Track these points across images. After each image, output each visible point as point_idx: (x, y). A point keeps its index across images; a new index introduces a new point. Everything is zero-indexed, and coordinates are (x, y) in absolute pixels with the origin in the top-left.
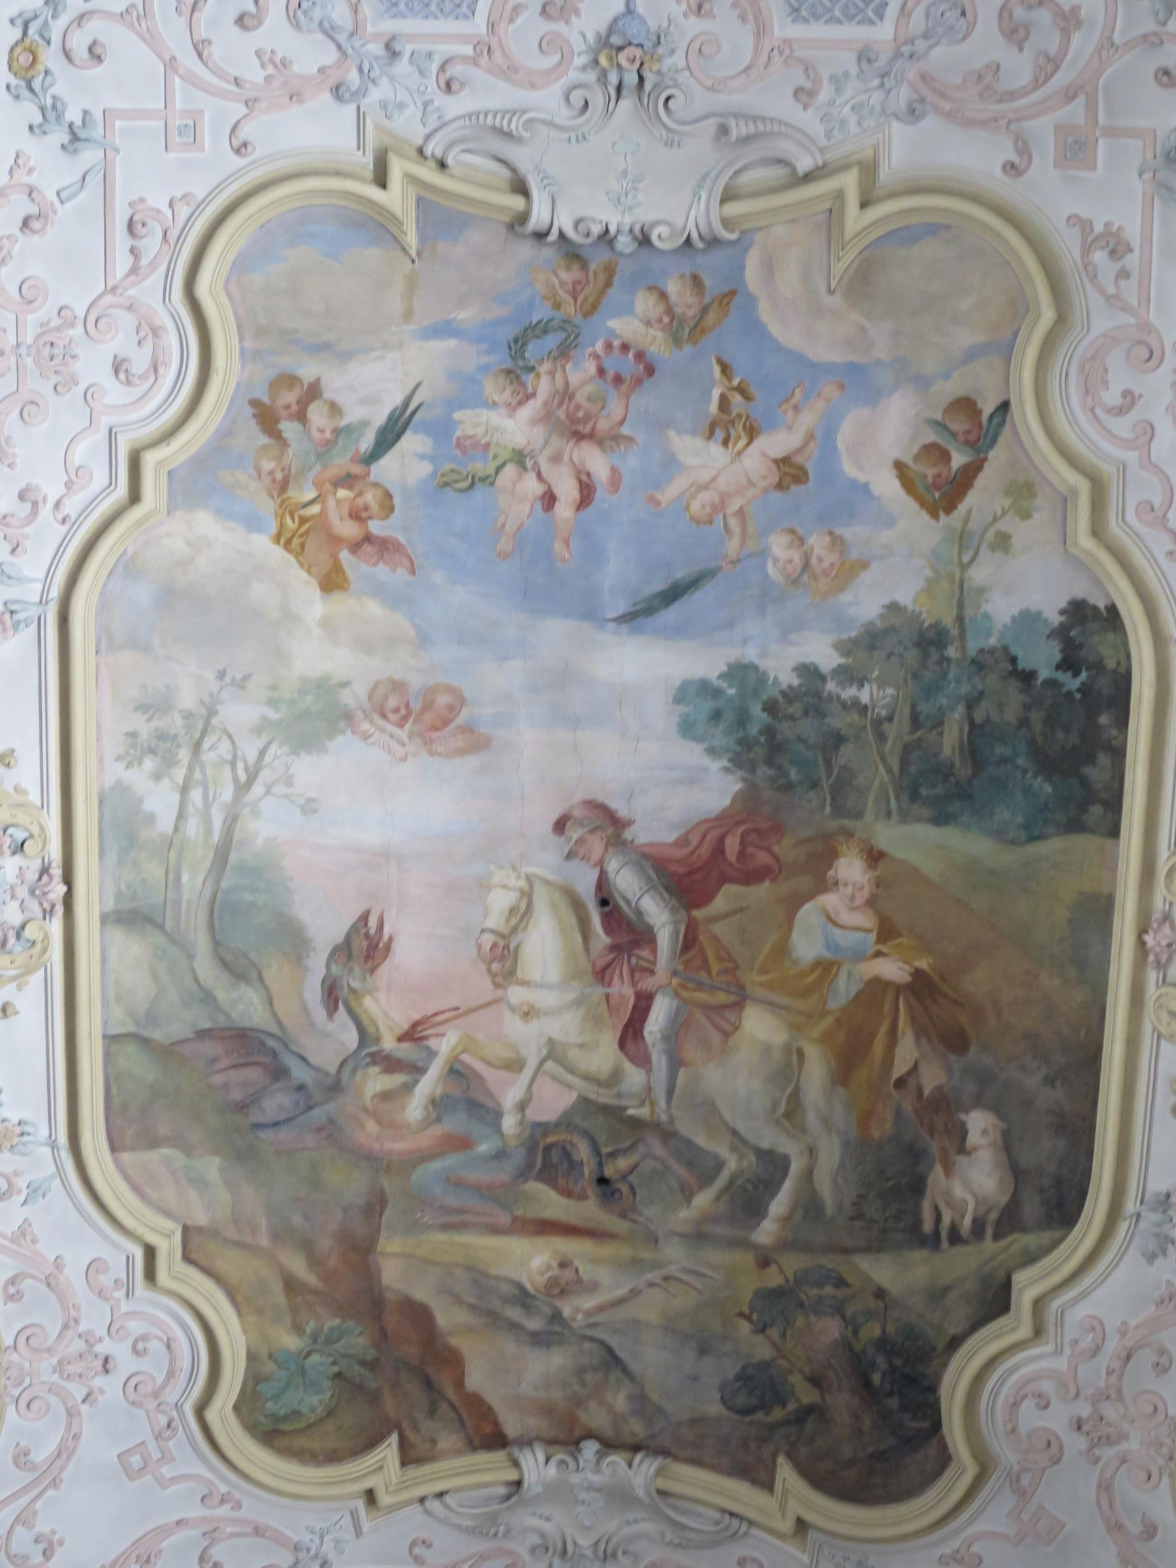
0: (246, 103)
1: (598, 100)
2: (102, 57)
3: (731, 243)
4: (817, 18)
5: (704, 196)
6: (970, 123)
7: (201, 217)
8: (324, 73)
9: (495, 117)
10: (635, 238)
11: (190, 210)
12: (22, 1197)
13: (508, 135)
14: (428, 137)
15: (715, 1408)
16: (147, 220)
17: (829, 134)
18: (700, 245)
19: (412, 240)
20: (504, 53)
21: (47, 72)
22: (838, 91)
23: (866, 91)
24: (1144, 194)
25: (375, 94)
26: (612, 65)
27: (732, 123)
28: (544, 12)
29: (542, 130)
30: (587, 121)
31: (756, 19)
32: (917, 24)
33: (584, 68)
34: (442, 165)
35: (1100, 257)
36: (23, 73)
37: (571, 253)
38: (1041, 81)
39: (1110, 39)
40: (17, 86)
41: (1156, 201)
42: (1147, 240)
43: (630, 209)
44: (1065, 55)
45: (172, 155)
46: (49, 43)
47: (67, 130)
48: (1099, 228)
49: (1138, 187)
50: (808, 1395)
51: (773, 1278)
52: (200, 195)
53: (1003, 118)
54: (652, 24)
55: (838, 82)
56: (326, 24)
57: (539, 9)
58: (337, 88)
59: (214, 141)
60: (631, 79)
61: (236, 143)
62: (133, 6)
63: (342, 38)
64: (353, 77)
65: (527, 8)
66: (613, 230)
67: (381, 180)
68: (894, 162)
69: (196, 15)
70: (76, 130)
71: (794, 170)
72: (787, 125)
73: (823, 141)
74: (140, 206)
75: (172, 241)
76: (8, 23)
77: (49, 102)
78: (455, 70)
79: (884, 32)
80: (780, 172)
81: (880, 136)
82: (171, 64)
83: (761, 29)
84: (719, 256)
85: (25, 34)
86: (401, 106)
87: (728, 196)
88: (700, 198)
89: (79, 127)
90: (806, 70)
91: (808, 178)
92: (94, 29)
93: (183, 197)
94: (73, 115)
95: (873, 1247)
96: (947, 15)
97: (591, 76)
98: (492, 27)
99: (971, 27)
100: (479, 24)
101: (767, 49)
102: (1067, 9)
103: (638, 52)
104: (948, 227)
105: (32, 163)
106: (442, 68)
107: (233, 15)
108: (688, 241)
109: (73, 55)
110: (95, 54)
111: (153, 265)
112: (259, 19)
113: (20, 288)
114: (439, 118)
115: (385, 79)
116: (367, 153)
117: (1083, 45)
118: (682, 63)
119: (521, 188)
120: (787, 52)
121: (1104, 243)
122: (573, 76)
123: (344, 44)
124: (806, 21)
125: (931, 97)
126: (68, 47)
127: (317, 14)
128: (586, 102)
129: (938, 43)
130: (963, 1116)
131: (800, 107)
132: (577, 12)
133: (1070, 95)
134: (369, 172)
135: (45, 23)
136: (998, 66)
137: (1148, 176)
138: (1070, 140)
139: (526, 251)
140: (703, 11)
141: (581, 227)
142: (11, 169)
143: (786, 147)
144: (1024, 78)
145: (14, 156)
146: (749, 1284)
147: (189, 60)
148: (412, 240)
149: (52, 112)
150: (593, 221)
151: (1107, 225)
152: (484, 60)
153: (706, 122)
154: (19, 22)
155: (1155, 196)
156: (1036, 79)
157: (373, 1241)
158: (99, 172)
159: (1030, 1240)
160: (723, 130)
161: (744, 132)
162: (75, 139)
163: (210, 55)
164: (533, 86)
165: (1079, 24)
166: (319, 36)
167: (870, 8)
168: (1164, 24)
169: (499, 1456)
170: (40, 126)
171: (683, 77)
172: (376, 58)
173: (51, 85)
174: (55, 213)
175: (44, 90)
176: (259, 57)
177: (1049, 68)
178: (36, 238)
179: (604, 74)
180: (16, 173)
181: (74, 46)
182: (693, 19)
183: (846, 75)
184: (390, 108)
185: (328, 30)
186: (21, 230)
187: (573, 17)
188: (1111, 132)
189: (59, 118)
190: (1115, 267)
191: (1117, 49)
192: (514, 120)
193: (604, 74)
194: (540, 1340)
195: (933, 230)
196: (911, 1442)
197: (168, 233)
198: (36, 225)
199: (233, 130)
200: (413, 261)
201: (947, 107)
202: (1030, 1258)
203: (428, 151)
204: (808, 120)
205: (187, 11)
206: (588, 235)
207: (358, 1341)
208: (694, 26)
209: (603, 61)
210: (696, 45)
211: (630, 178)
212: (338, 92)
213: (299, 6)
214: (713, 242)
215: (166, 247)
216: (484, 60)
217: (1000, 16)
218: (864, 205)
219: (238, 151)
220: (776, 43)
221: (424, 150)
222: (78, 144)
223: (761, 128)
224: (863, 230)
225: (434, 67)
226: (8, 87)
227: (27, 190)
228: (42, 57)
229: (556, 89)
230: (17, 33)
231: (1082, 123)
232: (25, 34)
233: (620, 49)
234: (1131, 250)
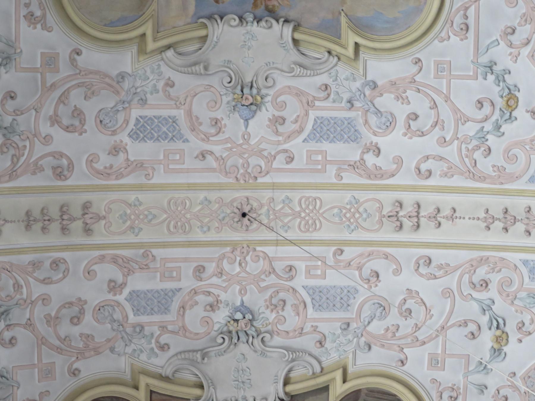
0: (415, 81)
1: (261, 82)
2: (477, 102)
3: (202, 18)
4: (165, 119)
5: (215, 39)
6: (97, 73)
7: (436, 32)
8: (381, 94)
9: (306, 74)
10: (245, 19)
11: (441, 35)
13: (301, 66)
14: (336, 65)
16: (460, 31)
17: (159, 66)
18: (216, 16)
19: (343, 20)
20: (301, 101)
21: (502, 97)
22: (155, 86)
23: (143, 86)
24: (19, 43)
25: (358, 84)
26: (255, 96)
27: (202, 71)
28: (284, 120)
29: (285, 68)
30: (265, 71)
31: (192, 118)
32: (121, 117)
33: (267, 95)
34: (329, 52)
35: (38, 13)
36: (513, 96)
37: (272, 13)
38: (66, 93)
39: (37, 112)
40: (515, 91)
41: (13, 38)
42: (17, 21)
43: (247, 33)
44: (56, 104)
45: (448, 59)
46: (501, 109)
47: (494, 71)
48: (39, 26)
49: (22, 45)
52: (436, 41)
53: (83, 75)
54: (237, 115)
55: (155, 90)
56: (379, 115)
57: (286, 121)
58: (375, 87)
59: (429, 64)
60: (246, 91)
61: (420, 64)
62: (463, 124)
63: (373, 109)
64: (368, 92)
65: (291, 122)
66: (255, 23)
67: (357, 45)
68: (130, 54)
69: (436, 120)
70: (490, 71)
71: (175, 50)
72: (178, 71)
73: (162, 63)
74: (462, 37)
75: (449, 21)
76: (518, 118)
77: (501, 84)
78: (323, 95)
79: (135, 113)
80: (181, 49)
81: (137, 66)
82: (447, 99)
83: (189, 113)
84: (207, 12)
85: (511, 113)
86: (347, 79)
87: (204, 39)
88: (217, 37)
89: (489, 72)
90: (169, 96)
91: (168, 47)
92: (480, 115)
93: (443, 41)
94: (491, 78)
96: (108, 121)
97: (264, 91)
98: (307, 114)
99: (97, 116)
100: (313, 115)
101: (186, 105)
102: (56, 125)
103: (244, 102)
104: (105, 25)
105: (510, 57)
106: (329, 95)
107: (420, 120)
108: (222, 18)
109: (490, 104)
110: (480, 104)
111: (458, 10)
112: (409, 117)
113: (517, 3)
114: (330, 74)
115: (354, 91)
116: (363, 58)
117: (48, 109)
118: (224, 97)
119: (295, 42)
120: (178, 103)
121: (36, 19)
122: (271, 92)
123: (372, 106)
124: (169, 117)
125: (114, 84)
126: (492, 107)
127: (383, 120)
128: (266, 80)
129: (112, 108)
131: (172, 79)
132: (270, 120)
133: (53, 86)
134: (362, 49)
135: (501, 118)
136: (85, 99)
137: (18, 51)
138: (53, 66)
139: (292, 14)
140: (215, 121)
141: (269, 25)
142: (519, 55)
143: (178, 61)
144: (73, 93)
145: (518, 61)
147: (439, 100)
148: (343, 20)
149: (500, 79)
150: (264, 28)
151: (35, 28)
152: (310, 99)
153: (214, 72)
154: (513, 119)
155: (14, 42)
156: (68, 93)
158: (481, 52)
160: (206, 68)
161: (197, 67)
162: (490, 67)
163: (430, 103)
164: (289, 87)
165: (51, 118)
166: (382, 110)
167: (142, 123)
168: (14, 120)
170: (506, 74)
171: (223, 91)
172: (358, 100)
173: (500, 91)
174: (500, 36)
175: (503, 89)
176: (409, 101)
177: (63, 98)
178: (509, 25)
179: (258, 93)
180: (517, 53)
181: (489, 107)
182: (219, 117)
183: (152, 93)
184: (352, 78)
185: (378, 112)
186: (516, 29)
187: (271, 118)
188: (34, 70)
189: (497, 77)
190: (32, 8)
191: (33, 108)
192: (298, 73)
193: (258, 93)
195: (111, 24)
197: (451, 25)
198: (510, 30)
199: (421, 70)
200: (342, 10)
201: (107, 80)
203: (336, 59)
204: (168, 73)
205: (440, 122)
206: (267, 21)
208: (218, 115)
209: (259, 98)
210: (218, 106)
211: (247, 47)
212: (374, 86)
213: (391, 123)
214: (210, 17)
215: (452, 19)
216: (310, 99)
217: (85, 120)
218: (144, 35)
219: (420, 60)
220: (183, 107)
221: (338, 59)
222: (490, 65)
223: (189, 69)
224: (144, 24)
225: (332, 96)
226: (519, 91)
227: (512, 46)
228: (504, 103)
229: (278, 87)
230: (514, 114)
231: (47, 74)
232: (511, 113)
233: (251, 104)
234: (24, 16)
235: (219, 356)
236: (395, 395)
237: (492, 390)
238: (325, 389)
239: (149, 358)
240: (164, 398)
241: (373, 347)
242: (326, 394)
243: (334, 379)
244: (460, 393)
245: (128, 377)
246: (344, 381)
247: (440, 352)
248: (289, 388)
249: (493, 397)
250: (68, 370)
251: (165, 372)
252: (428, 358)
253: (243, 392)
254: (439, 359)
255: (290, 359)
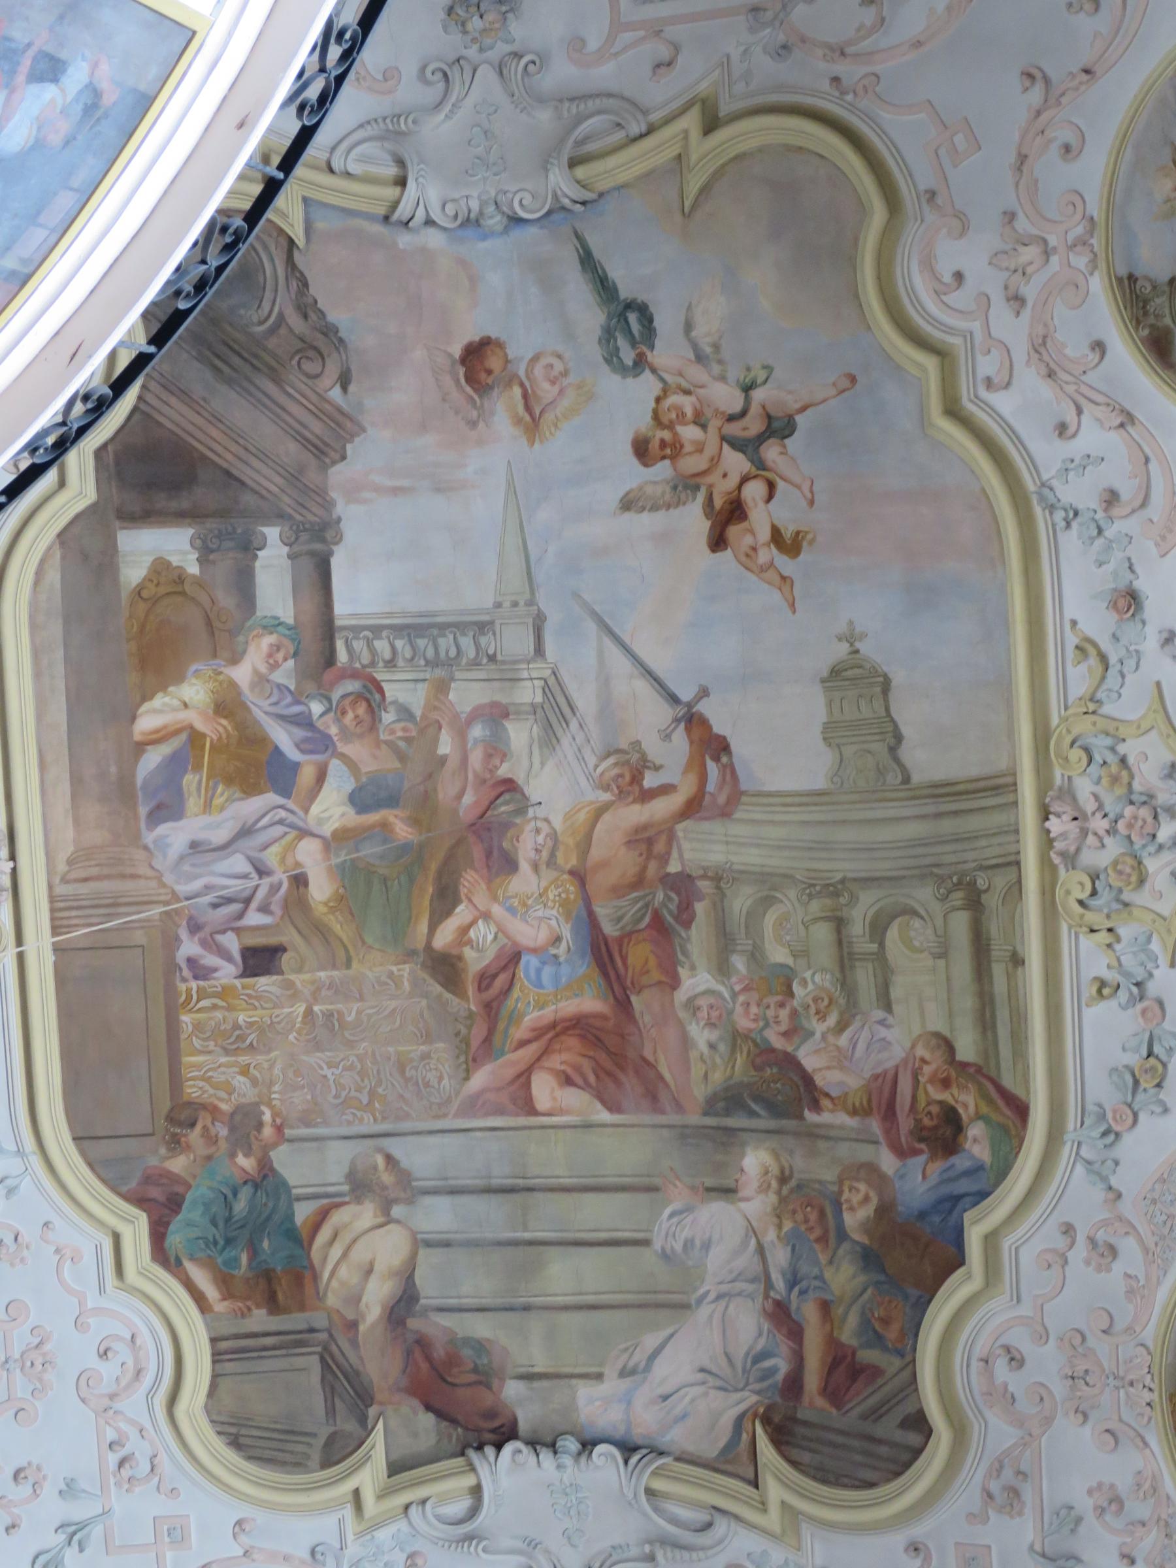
235: (621, 1547)
236: (250, 1458)
237: (49, 1491)
238: (395, 1468)
239: (764, 1553)
240: (729, 1468)
241: (306, 1555)
242: (394, 1456)
243: (381, 1496)
244: (115, 1476)
245: (806, 1530)
246: (356, 1493)
247: (169, 1555)
248: (470, 1480)
249: (44, 1478)
250: (931, 1558)
251: (729, 1526)
252: (197, 450)
253: (565, 1478)
254: (167, 1539)
255: (474, 1542)
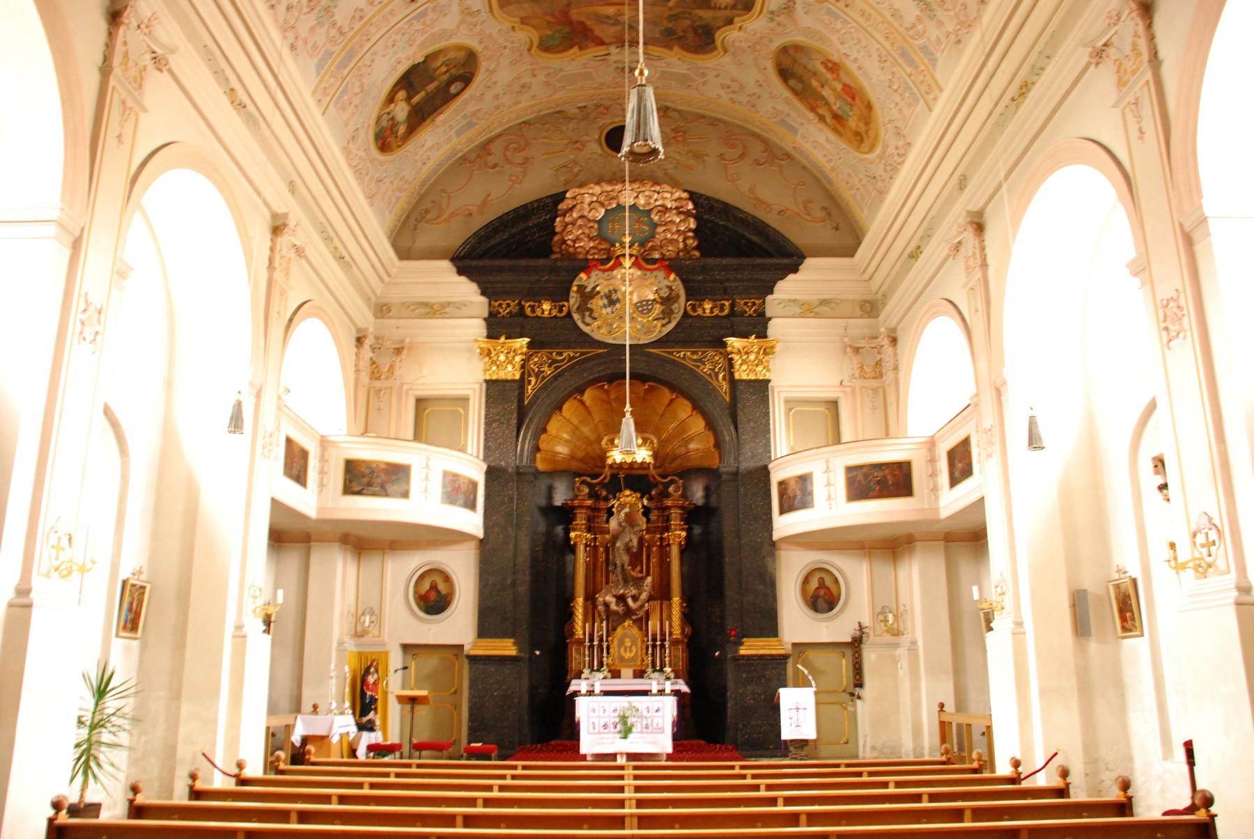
12: (626, 566)
15: (657, 35)
31: (595, 607)
50: (682, 34)
51: (672, 13)
95: (700, 8)
130: (610, 461)
146: (667, 13)
157: (569, 11)
159: (738, 12)
169: (604, 47)
194: (614, 25)
196: (708, 44)
202: (739, 16)
207: (566, 30)
